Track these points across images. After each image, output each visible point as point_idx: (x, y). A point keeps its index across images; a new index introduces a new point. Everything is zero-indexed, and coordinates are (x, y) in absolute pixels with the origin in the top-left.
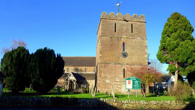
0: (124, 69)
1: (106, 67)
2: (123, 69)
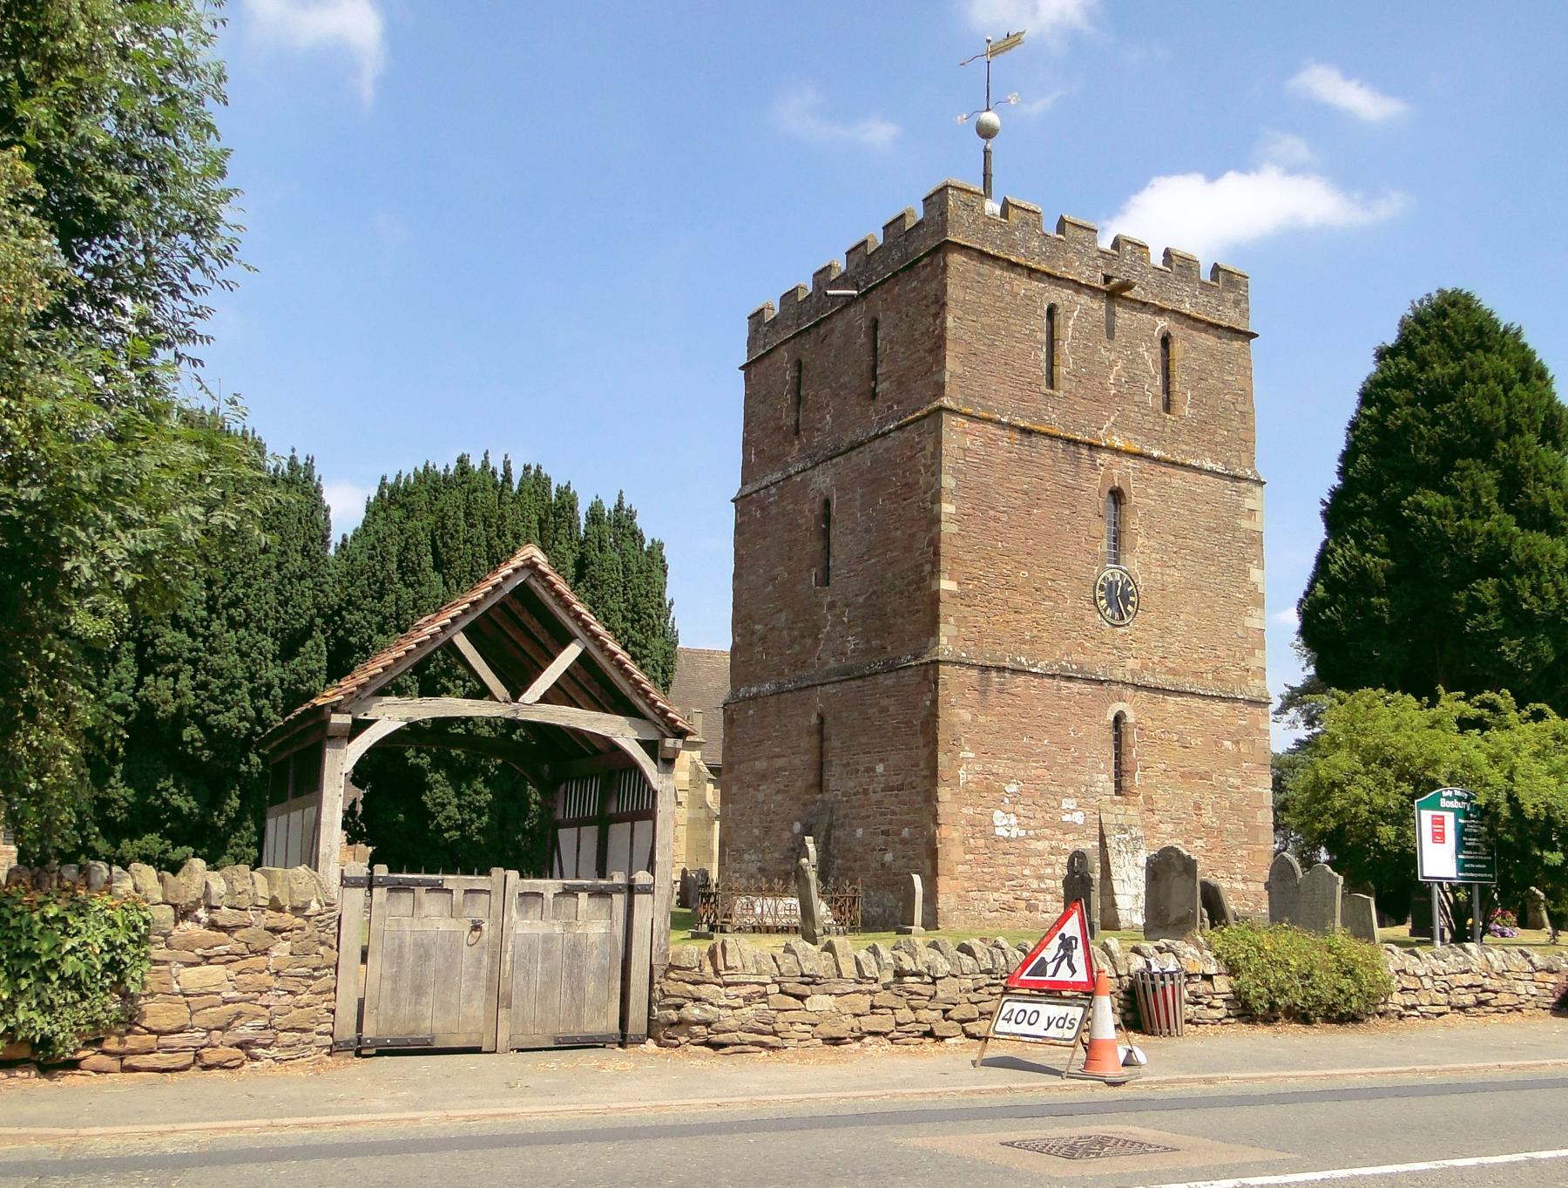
0: (1119, 719)
1: (992, 698)
2: (1111, 718)
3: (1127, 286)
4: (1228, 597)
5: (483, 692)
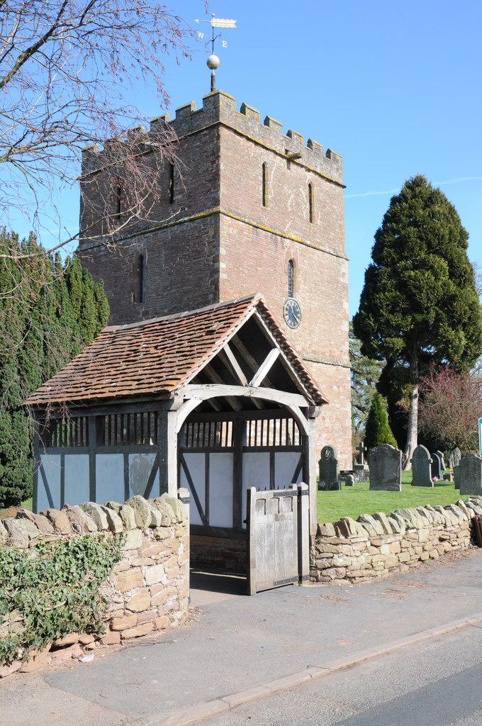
3: (298, 157)
4: (335, 315)
5: (234, 381)
